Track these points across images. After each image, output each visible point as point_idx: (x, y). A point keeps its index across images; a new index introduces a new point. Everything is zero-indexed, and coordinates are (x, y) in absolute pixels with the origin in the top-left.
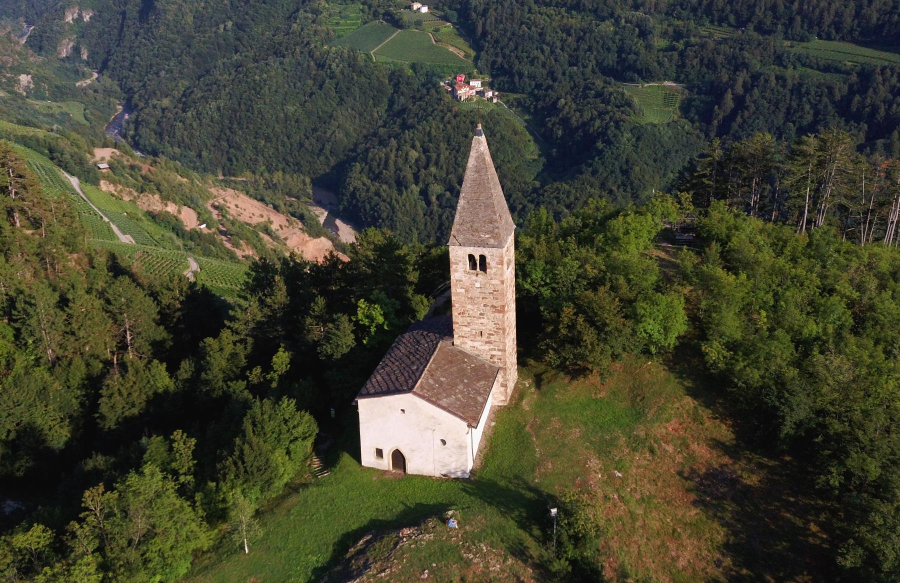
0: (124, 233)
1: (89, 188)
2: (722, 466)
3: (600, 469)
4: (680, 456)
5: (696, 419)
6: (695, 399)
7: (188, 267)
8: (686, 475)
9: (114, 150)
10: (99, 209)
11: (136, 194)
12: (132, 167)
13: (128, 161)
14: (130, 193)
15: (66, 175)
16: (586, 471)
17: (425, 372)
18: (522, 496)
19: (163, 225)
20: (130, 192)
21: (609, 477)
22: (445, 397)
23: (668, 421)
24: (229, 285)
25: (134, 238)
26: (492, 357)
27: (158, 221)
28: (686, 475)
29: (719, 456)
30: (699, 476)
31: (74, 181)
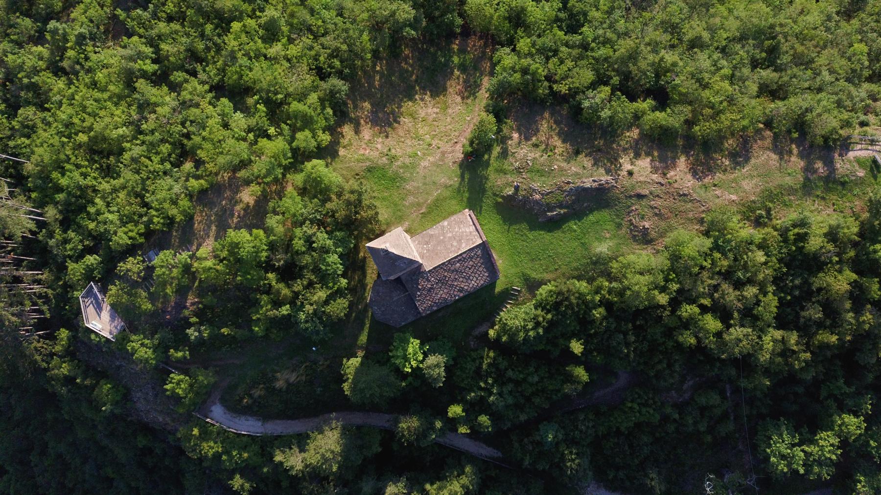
18: (469, 179)
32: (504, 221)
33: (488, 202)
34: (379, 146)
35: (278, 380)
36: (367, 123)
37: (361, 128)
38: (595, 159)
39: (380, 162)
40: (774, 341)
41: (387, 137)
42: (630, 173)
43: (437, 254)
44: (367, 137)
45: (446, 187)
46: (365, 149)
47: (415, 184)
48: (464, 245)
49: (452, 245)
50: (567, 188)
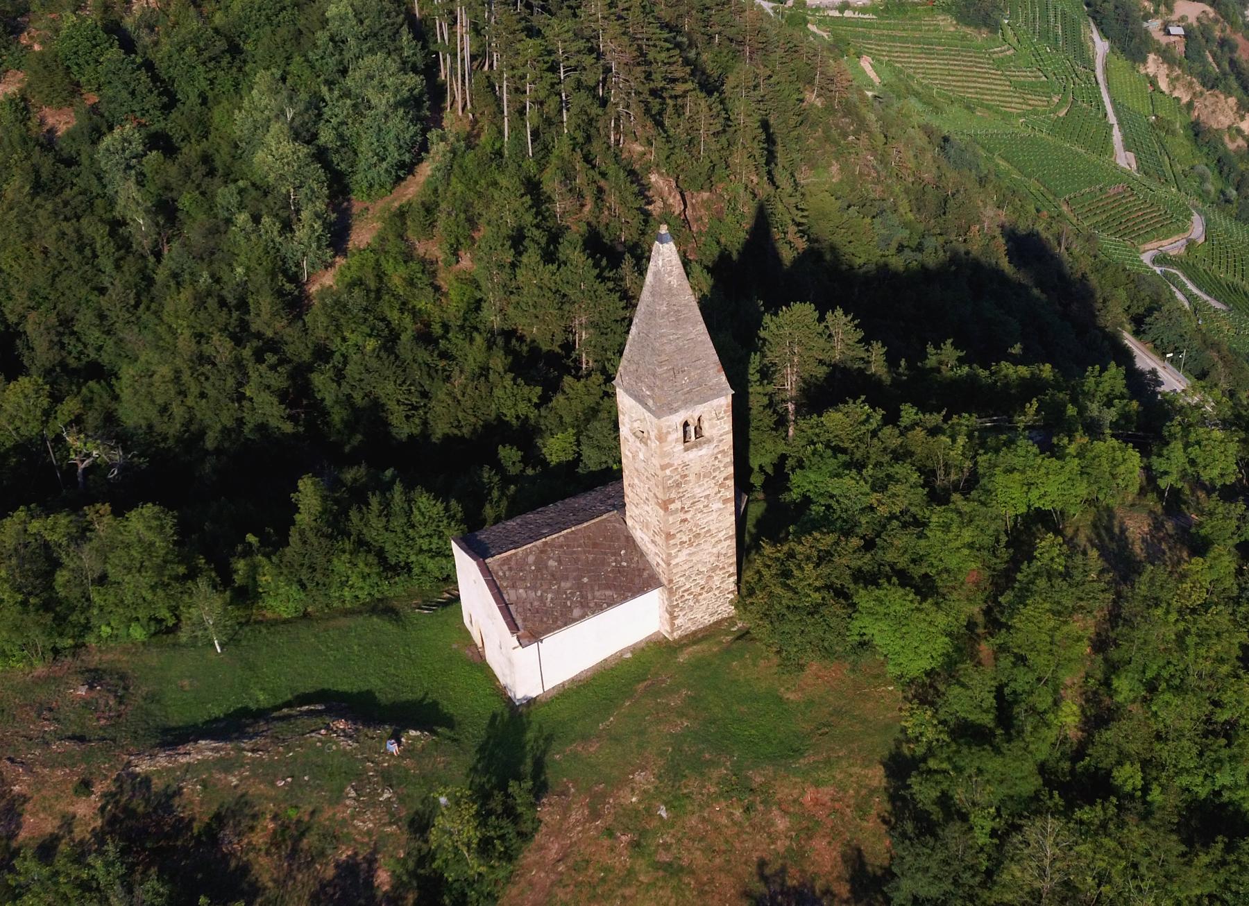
0: (1127, 148)
1: (1121, 63)
2: (827, 892)
3: (645, 792)
4: (787, 843)
5: (861, 809)
6: (887, 776)
7: (1184, 231)
8: (767, 872)
9: (1208, 9)
10: (1113, 102)
11: (1198, 88)
12: (1223, 43)
13: (1222, 31)
14: (1190, 85)
15: (1096, 35)
16: (623, 782)
17: (539, 543)
18: (521, 761)
19: (1205, 150)
20: (1191, 83)
21: (647, 810)
22: (526, 588)
23: (817, 784)
24: (1230, 277)
25: (1138, 159)
26: (658, 564)
27: (1200, 141)
28: (767, 872)
29: (839, 878)
30: (783, 884)
31: (1100, 46)
32: (435, 704)
33: (475, 733)
34: (781, 824)
35: (254, 141)
36: (827, 892)
37: (843, 870)
38: (169, 809)
39: (770, 771)
40: (472, 161)
41: (762, 864)
42: (85, 786)
43: (595, 545)
44: (819, 844)
45: (585, 738)
46: (816, 802)
47: (664, 729)
48: (531, 559)
49: (560, 562)
50: (260, 741)
